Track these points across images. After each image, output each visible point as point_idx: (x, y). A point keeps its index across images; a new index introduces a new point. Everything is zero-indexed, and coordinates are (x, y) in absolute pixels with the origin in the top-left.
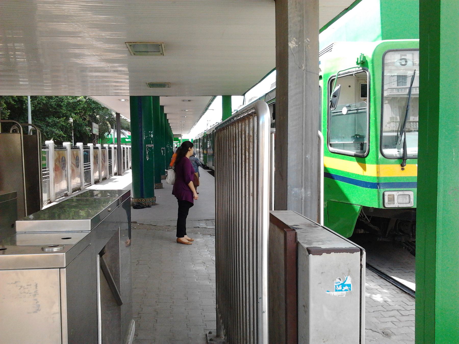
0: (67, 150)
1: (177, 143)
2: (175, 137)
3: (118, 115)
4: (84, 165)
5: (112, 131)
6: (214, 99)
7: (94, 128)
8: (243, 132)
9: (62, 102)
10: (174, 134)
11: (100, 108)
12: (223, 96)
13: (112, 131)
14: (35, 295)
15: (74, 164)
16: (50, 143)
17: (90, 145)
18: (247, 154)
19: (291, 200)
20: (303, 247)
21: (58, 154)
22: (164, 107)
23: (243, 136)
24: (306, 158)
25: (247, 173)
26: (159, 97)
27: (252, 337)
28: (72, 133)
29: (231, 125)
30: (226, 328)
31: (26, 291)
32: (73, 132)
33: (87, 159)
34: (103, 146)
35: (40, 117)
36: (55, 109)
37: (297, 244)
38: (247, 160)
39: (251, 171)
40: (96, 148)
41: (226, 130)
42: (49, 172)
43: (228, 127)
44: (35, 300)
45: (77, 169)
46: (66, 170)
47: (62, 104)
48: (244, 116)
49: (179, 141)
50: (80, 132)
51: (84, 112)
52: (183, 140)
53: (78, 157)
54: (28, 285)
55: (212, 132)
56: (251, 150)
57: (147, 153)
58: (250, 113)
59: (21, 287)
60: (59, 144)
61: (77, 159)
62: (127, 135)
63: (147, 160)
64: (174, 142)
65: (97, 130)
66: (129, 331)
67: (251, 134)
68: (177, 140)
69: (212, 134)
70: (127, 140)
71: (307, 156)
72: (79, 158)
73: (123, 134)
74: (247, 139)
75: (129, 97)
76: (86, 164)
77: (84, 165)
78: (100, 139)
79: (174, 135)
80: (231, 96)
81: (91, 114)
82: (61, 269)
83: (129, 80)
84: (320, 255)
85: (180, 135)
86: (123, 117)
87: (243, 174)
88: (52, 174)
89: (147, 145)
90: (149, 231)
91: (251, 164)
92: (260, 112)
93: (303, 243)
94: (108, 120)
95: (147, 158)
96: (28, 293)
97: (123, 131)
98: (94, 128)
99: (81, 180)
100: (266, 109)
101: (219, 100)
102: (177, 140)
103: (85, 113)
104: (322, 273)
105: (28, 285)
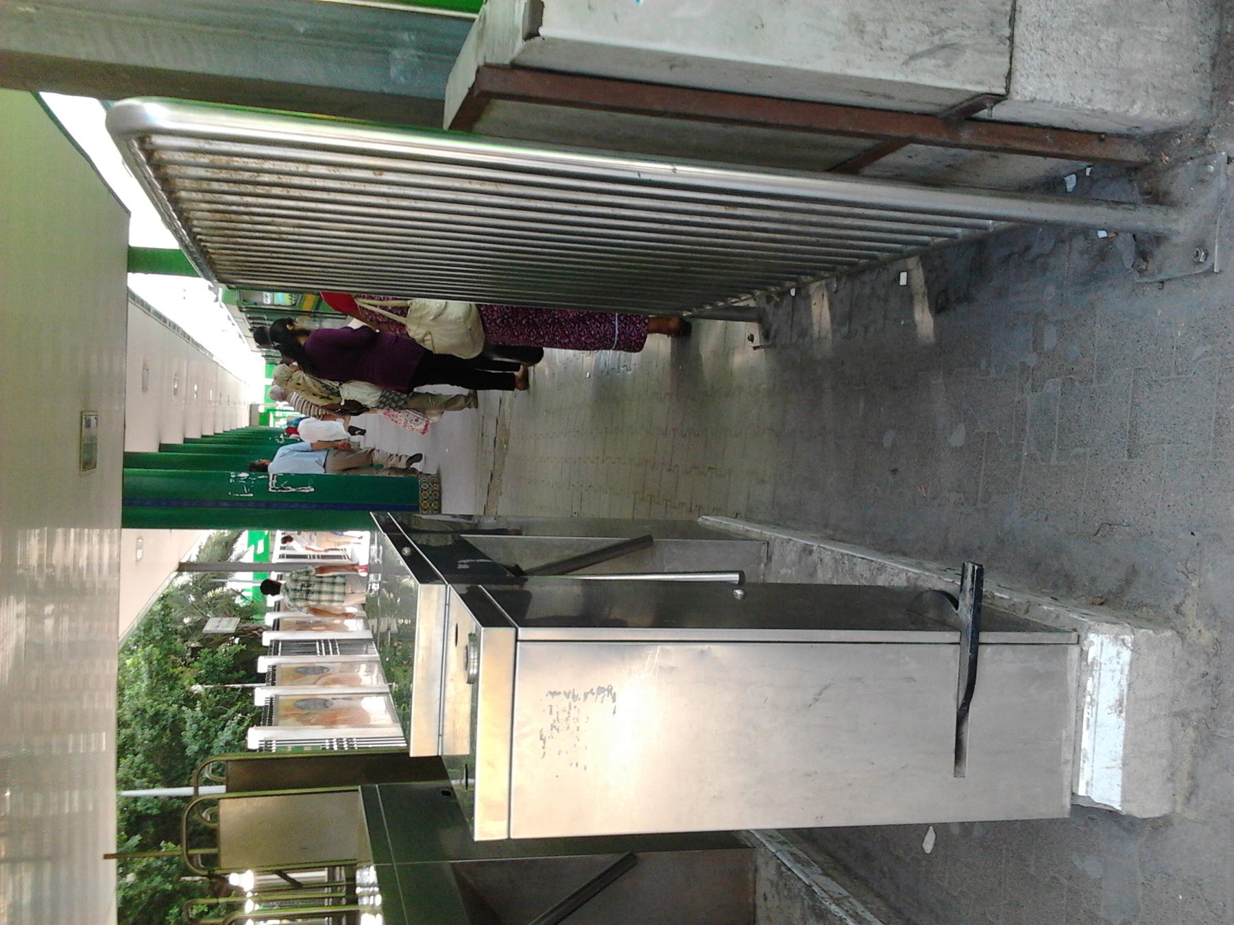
0: (277, 696)
1: (275, 417)
2: (256, 422)
3: (182, 568)
4: (321, 653)
5: (231, 585)
6: (134, 297)
7: (218, 629)
8: (205, 185)
9: (144, 711)
10: (247, 425)
11: (163, 615)
12: (128, 271)
13: (231, 585)
14: (575, 697)
15: (319, 678)
16: (256, 737)
17: (267, 638)
18: (266, 178)
19: (419, 87)
20: (523, 51)
21: (286, 716)
22: (163, 442)
23: (215, 186)
24: (305, 34)
25: (320, 183)
26: (124, 453)
27: (739, 211)
28: (233, 689)
29: (190, 223)
30: (736, 291)
31: (563, 716)
32: (231, 686)
33: (307, 647)
34: (271, 608)
35: (184, 768)
36: (164, 728)
37: (515, 66)
38: (285, 179)
39: (313, 169)
40: (277, 626)
41: (208, 244)
42: (335, 740)
43: (199, 237)
44: (586, 695)
45: (331, 671)
46: (333, 699)
47: (151, 712)
48: (155, 178)
49: (268, 411)
50: (229, 670)
51: (173, 657)
52: (266, 400)
53: (300, 670)
54: (551, 713)
55: (243, 314)
56: (252, 163)
57: (294, 490)
58: (145, 157)
59: (553, 727)
60: (263, 717)
61: (301, 674)
62: (246, 546)
63: (313, 490)
64: (271, 425)
65: (226, 620)
66: (722, 527)
67: (205, 160)
68: (265, 418)
69: (248, 316)
70: (261, 550)
71: (302, 30)
72: (302, 665)
73: (240, 557)
74: (224, 175)
75: (124, 530)
76: (321, 651)
77: (321, 653)
78: (254, 617)
79: (250, 425)
80: (129, 247)
81: (179, 639)
82: (520, 637)
83: (71, 527)
84: (544, 6)
85: (253, 408)
86: (192, 555)
87: (325, 195)
88: (342, 732)
89: (270, 490)
90: (503, 491)
91: (292, 167)
92: (139, 125)
93: (513, 51)
94: (199, 596)
95: (307, 491)
96: (569, 713)
97: (233, 558)
98: (218, 629)
99: (364, 662)
100: (129, 107)
101: (139, 283)
102: (265, 418)
103: (176, 653)
104: (590, 8)
105: (551, 713)
